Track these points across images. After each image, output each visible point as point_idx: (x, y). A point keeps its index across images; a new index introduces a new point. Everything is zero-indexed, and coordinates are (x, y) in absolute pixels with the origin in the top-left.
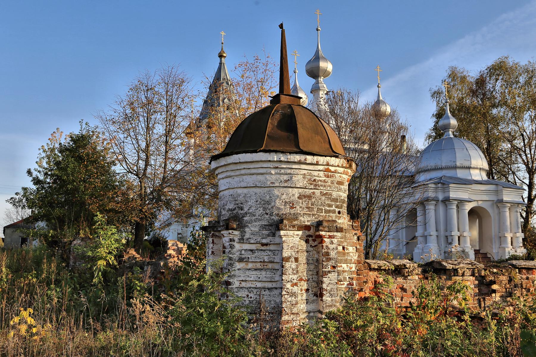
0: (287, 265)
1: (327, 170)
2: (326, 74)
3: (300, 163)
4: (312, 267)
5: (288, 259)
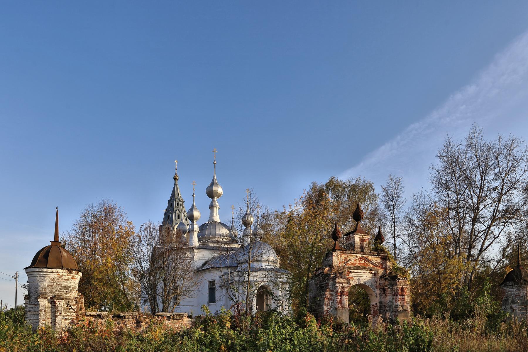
0: (41, 313)
1: (58, 275)
2: (219, 196)
3: (46, 272)
4: (53, 314)
5: (41, 310)
